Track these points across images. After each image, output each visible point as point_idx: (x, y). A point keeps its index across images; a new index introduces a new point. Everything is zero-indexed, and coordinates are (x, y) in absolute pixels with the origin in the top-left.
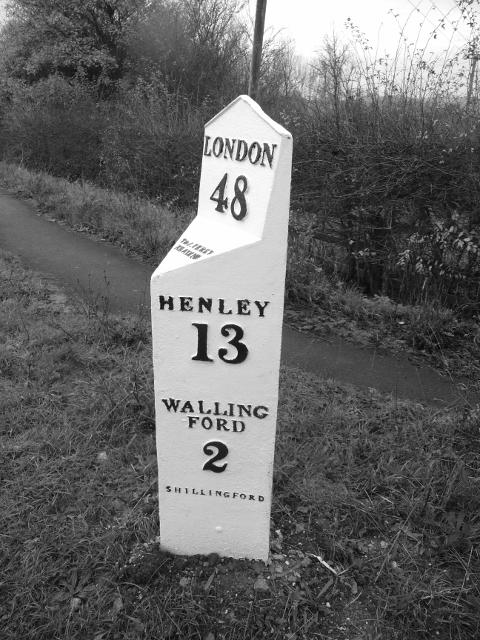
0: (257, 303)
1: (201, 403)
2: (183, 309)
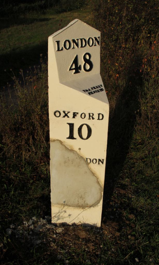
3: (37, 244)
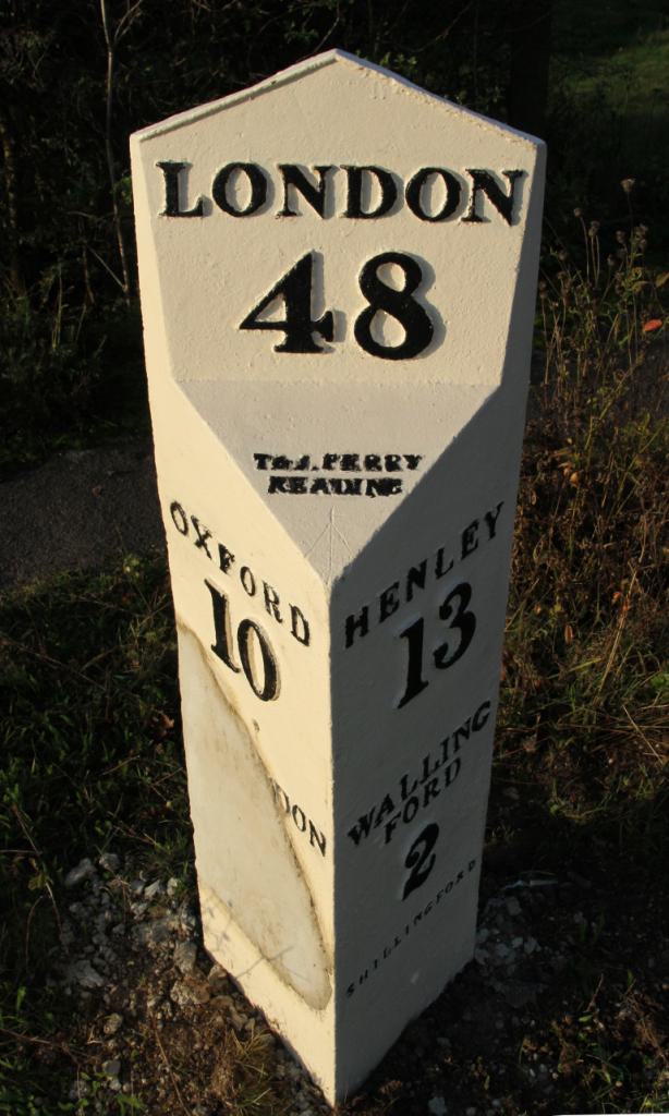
3: (82, 983)
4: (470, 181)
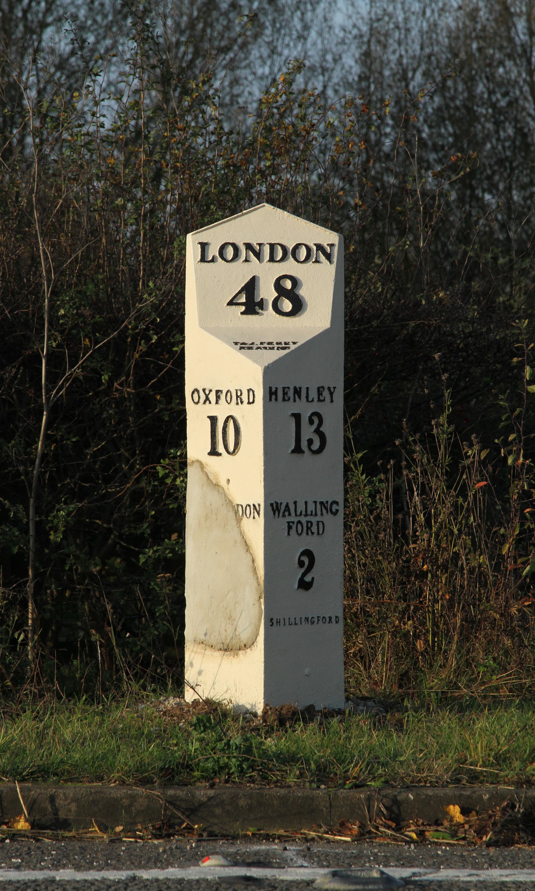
0: (329, 388)
1: (295, 503)
2: (284, 400)
4: (315, 248)
